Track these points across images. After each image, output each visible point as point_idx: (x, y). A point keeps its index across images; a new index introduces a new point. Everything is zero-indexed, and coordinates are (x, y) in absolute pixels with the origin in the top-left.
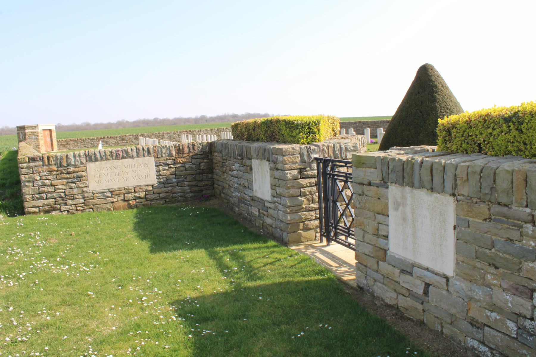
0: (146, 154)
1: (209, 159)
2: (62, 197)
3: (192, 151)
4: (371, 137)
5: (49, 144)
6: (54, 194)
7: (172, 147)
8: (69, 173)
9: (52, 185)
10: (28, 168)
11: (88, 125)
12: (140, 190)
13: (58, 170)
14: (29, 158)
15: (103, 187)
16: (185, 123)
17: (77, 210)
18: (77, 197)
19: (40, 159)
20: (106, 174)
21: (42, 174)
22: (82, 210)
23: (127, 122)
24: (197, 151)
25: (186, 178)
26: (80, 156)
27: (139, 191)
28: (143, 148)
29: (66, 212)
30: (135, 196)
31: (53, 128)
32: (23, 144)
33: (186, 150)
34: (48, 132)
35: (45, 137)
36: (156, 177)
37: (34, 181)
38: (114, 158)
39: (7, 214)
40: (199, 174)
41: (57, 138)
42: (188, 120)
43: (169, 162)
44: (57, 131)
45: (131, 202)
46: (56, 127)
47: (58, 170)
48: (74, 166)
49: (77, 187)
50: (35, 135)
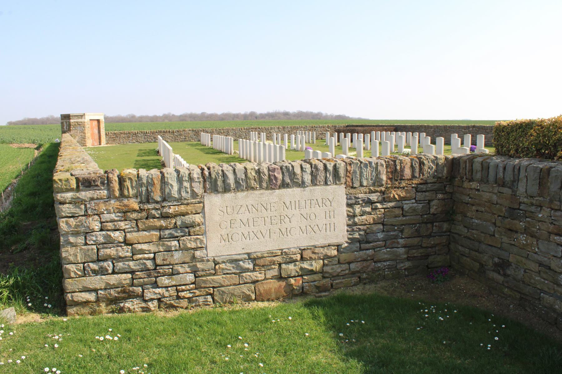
0: (331, 178)
1: (446, 193)
2: (149, 270)
3: (417, 175)
4: (472, 144)
5: (97, 137)
6: (131, 263)
7: (382, 165)
8: (165, 216)
9: (126, 242)
10: (76, 202)
11: (133, 117)
12: (313, 256)
13: (141, 210)
14: (77, 179)
15: (237, 249)
16: (233, 119)
17: (178, 297)
18: (181, 270)
19: (103, 183)
20: (245, 221)
21: (106, 217)
22: (189, 298)
23: (173, 115)
24: (426, 175)
25: (402, 231)
26: (191, 179)
27: (311, 259)
28: (325, 166)
29: (155, 302)
30: (301, 269)
31: (102, 118)
32: (67, 136)
33: (408, 172)
34: (96, 122)
35: (92, 128)
36: (346, 228)
37: (87, 233)
38: (264, 185)
39: (25, 303)
40: (426, 223)
41: (105, 130)
42: (236, 116)
43: (374, 197)
44: (105, 122)
45: (292, 281)
46: (106, 118)
47: (141, 210)
48: (177, 200)
49: (180, 249)
50: (81, 125)
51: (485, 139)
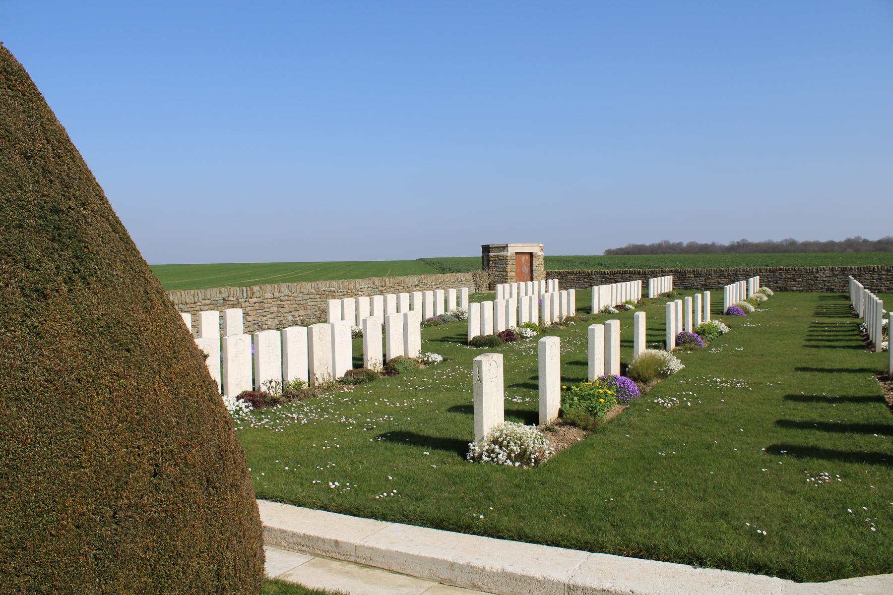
11: (793, 243)
23: (865, 241)
34: (527, 257)
36: (496, 425)
50: (503, 260)
51: (577, 300)
